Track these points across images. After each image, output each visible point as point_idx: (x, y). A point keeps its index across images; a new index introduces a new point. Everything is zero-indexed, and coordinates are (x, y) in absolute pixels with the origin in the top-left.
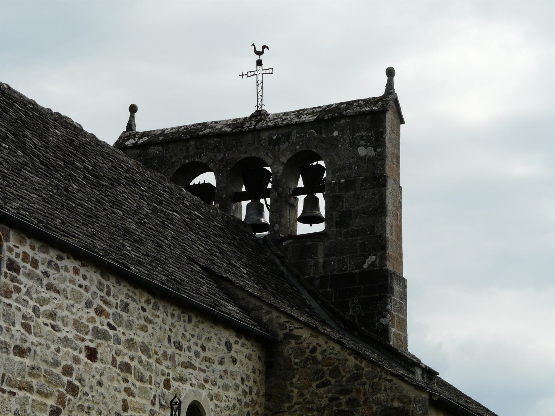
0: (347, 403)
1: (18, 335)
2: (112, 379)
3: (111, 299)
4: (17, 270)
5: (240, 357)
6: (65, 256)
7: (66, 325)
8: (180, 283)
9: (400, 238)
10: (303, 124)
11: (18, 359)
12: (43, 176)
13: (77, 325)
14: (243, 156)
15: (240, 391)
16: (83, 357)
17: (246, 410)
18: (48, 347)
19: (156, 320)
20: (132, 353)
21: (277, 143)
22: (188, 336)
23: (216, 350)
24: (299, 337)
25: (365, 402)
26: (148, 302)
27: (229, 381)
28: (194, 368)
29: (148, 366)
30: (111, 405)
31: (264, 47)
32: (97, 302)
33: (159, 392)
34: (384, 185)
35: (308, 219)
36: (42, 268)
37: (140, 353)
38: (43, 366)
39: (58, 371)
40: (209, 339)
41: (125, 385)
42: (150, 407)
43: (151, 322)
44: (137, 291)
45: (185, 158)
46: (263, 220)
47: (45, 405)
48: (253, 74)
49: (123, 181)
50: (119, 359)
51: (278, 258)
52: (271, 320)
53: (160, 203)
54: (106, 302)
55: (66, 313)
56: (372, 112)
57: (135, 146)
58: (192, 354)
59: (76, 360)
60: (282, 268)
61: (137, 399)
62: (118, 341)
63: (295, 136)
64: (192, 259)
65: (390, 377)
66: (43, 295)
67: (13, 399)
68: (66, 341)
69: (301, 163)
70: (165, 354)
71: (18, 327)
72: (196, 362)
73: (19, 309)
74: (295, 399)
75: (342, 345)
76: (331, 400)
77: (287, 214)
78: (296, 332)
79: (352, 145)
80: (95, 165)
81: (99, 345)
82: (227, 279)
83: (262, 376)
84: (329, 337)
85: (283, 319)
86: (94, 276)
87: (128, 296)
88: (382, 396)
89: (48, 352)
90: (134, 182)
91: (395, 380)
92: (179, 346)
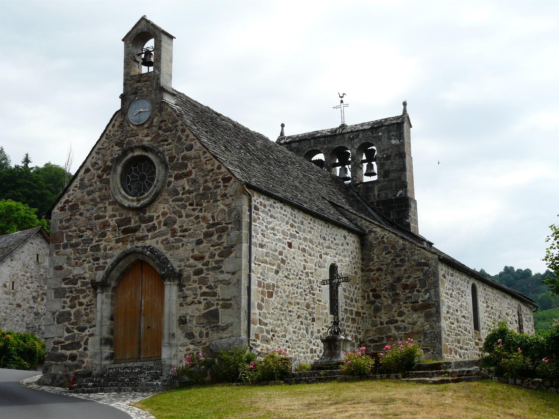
0: (400, 261)
1: (260, 239)
2: (298, 256)
3: (296, 220)
4: (258, 210)
5: (350, 242)
6: (276, 202)
7: (279, 233)
8: (322, 210)
9: (413, 182)
10: (364, 130)
11: (261, 249)
12: (259, 164)
13: (283, 233)
14: (337, 146)
15: (351, 258)
16: (286, 246)
17: (354, 266)
18: (272, 243)
19: (315, 228)
20: (306, 244)
21: (352, 139)
22: (328, 234)
23: (340, 239)
24: (375, 232)
25: (408, 260)
26: (311, 220)
27: (346, 253)
28: (331, 248)
30: (299, 267)
31: (344, 94)
32: (291, 221)
33: (318, 260)
34: (405, 157)
35: (369, 174)
36: (268, 208)
37: (309, 243)
38: (271, 252)
39: (277, 253)
40: (337, 235)
41: (304, 258)
42: (314, 267)
43: (313, 229)
44: (306, 215)
45: (309, 148)
46: (347, 176)
47: (273, 269)
48: (339, 107)
49: (289, 163)
51: (357, 193)
52: (362, 224)
53: (305, 172)
54: (294, 221)
55: (279, 227)
56: (397, 123)
57: (285, 143)
58: (330, 242)
59: (284, 248)
60: (358, 198)
61: (309, 264)
62: (300, 239)
63: (361, 136)
64: (323, 198)
65: (419, 249)
66: (269, 220)
67: (260, 267)
68: (279, 240)
69: (364, 148)
70: (319, 243)
71: (260, 235)
72: (332, 246)
73: (260, 227)
74: (375, 260)
75: (396, 234)
76: (392, 260)
77: (358, 172)
78: (374, 229)
79: (387, 140)
80: (277, 156)
81: (293, 241)
82: (340, 206)
83: (360, 250)
84: (389, 231)
85: (368, 224)
86: (289, 210)
87: (303, 218)
88: (416, 257)
89: (272, 245)
90: (293, 163)
91: (422, 250)
92: (324, 239)
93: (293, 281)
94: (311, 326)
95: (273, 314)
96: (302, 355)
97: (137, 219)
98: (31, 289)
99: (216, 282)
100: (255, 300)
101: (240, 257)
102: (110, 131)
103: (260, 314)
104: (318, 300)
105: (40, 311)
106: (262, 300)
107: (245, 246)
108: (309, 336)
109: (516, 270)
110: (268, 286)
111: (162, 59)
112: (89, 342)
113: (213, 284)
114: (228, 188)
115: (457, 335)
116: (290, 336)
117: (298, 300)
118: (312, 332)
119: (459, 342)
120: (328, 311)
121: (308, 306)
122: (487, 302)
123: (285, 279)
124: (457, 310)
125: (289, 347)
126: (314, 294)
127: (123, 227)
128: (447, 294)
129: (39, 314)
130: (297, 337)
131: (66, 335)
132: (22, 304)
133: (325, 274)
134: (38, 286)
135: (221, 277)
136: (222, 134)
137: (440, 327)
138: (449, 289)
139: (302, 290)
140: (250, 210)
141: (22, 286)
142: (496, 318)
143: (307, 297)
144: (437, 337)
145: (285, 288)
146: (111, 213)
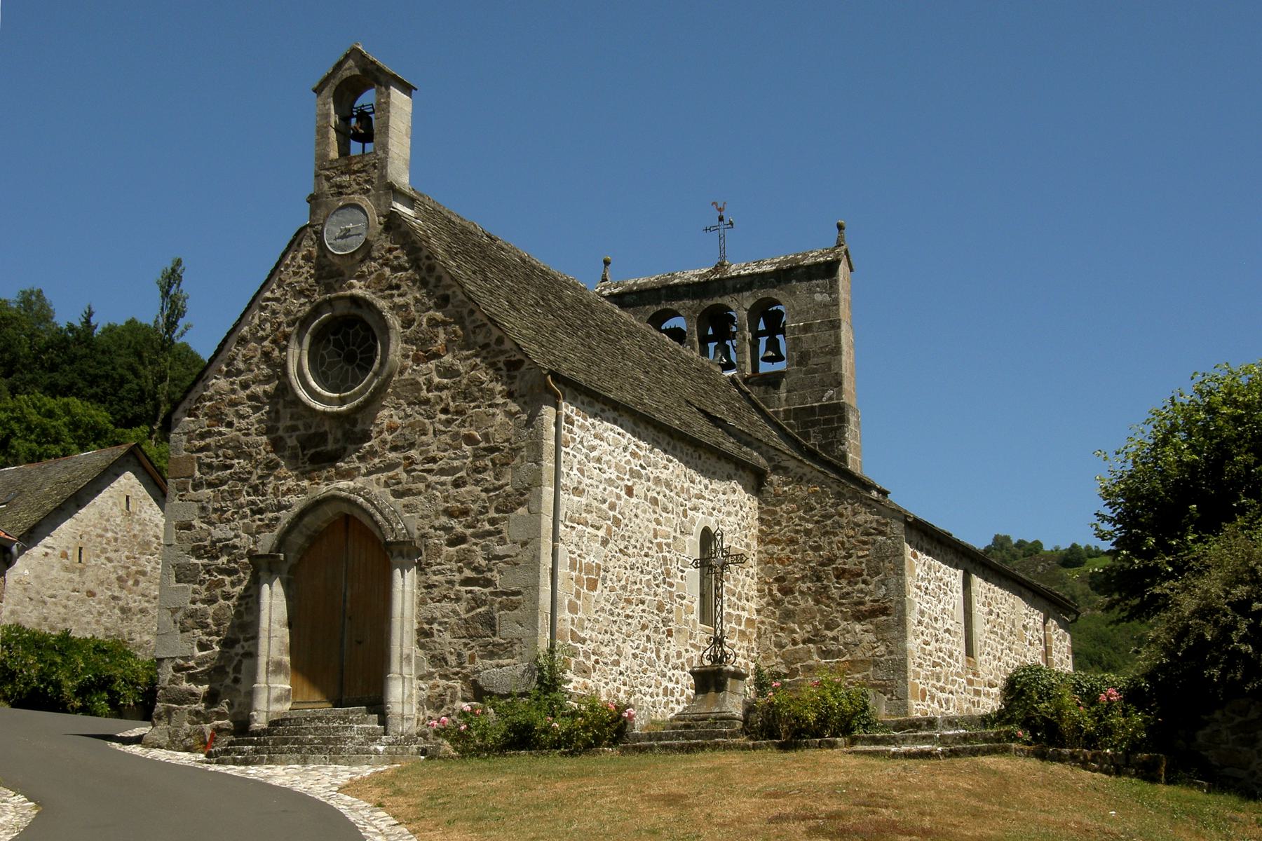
2: (645, 512)
4: (572, 424)
13: (618, 468)
16: (623, 493)
28: (704, 498)
29: (671, 499)
34: (839, 327)
38: (595, 503)
39: (605, 506)
44: (660, 435)
48: (716, 228)
50: (649, 494)
54: (638, 446)
56: (826, 262)
59: (619, 497)
68: (610, 482)
71: (575, 471)
78: (783, 464)
81: (634, 483)
89: (598, 491)
90: (631, 333)
93: (633, 560)
94: (667, 645)
95: (597, 621)
96: (648, 698)
97: (339, 434)
98: (116, 563)
99: (489, 560)
100: (564, 598)
101: (539, 514)
102: (287, 266)
103: (573, 620)
104: (679, 596)
105: (132, 605)
106: (578, 596)
107: (548, 491)
108: (662, 663)
109: (1014, 541)
110: (589, 568)
111: (391, 129)
112: (243, 667)
113: (484, 563)
114: (517, 382)
115: (935, 665)
116: (628, 663)
117: (643, 596)
118: (667, 656)
119: (938, 680)
120: (696, 616)
121: (660, 608)
122: (990, 604)
123: (619, 555)
124: (936, 619)
125: (625, 684)
126: (671, 585)
127: (313, 451)
128: (919, 587)
129: (130, 609)
130: (640, 666)
131: (198, 654)
132: (97, 590)
133: (692, 547)
134: (128, 558)
135: (499, 550)
136: (501, 276)
137: (905, 651)
138: (923, 579)
139: (650, 577)
140: (557, 424)
141: (98, 556)
142: (1005, 633)
143: (660, 591)
144: (900, 667)
145: (617, 571)
146: (289, 423)
